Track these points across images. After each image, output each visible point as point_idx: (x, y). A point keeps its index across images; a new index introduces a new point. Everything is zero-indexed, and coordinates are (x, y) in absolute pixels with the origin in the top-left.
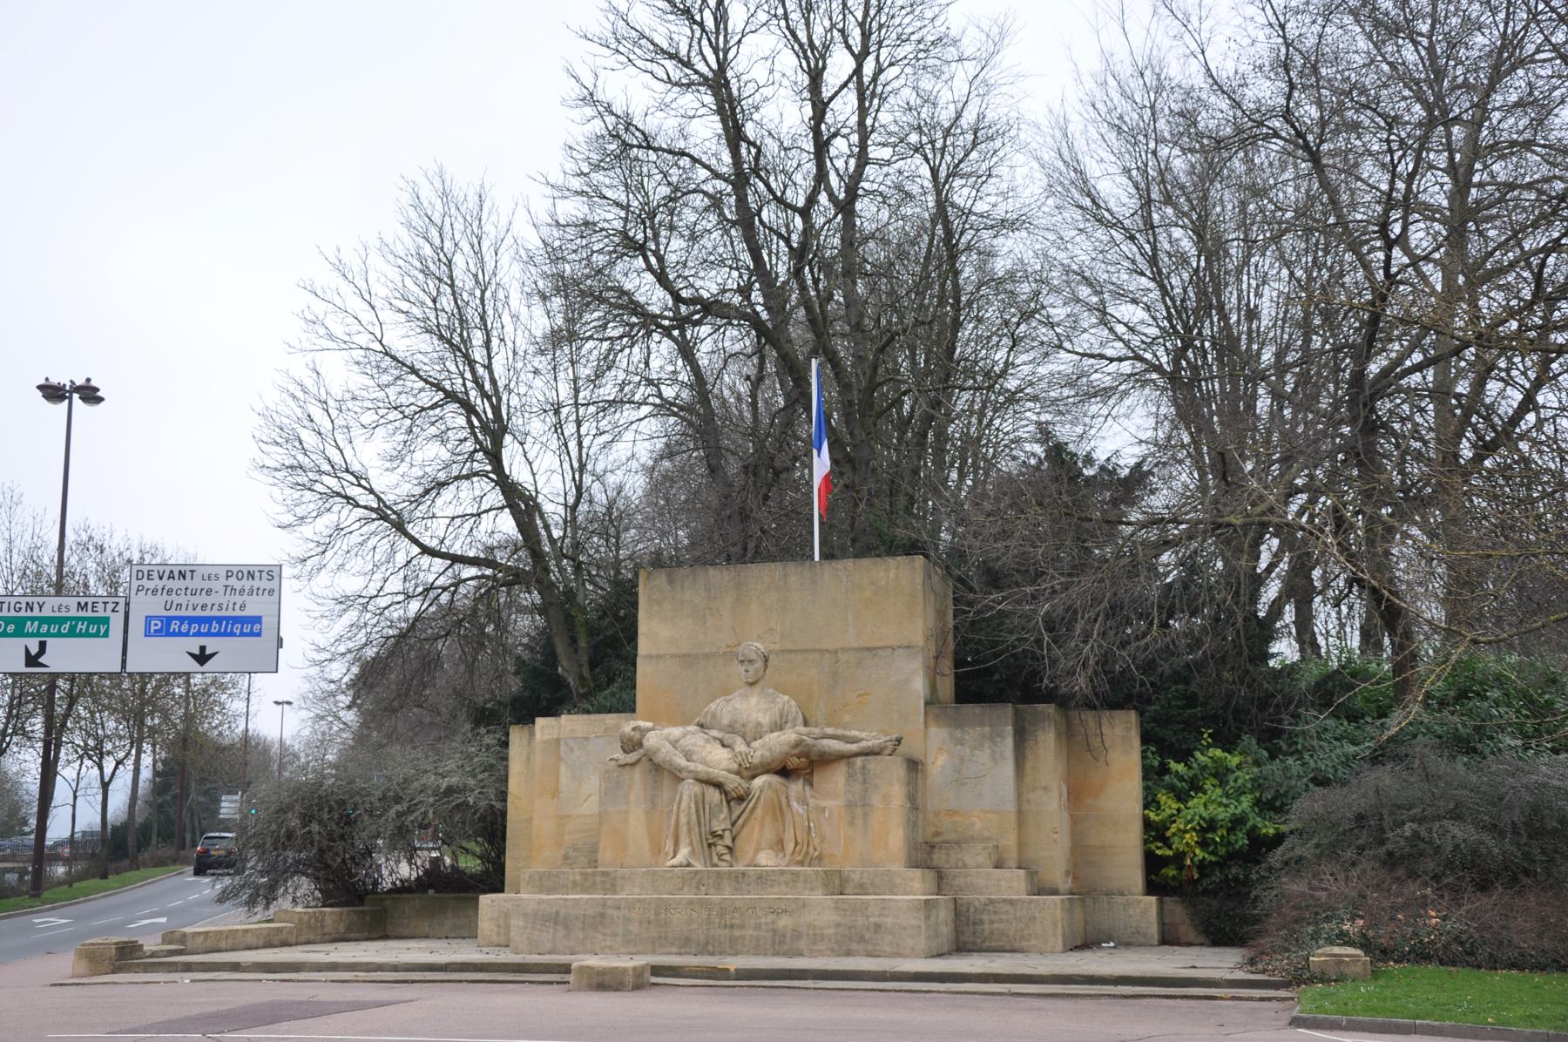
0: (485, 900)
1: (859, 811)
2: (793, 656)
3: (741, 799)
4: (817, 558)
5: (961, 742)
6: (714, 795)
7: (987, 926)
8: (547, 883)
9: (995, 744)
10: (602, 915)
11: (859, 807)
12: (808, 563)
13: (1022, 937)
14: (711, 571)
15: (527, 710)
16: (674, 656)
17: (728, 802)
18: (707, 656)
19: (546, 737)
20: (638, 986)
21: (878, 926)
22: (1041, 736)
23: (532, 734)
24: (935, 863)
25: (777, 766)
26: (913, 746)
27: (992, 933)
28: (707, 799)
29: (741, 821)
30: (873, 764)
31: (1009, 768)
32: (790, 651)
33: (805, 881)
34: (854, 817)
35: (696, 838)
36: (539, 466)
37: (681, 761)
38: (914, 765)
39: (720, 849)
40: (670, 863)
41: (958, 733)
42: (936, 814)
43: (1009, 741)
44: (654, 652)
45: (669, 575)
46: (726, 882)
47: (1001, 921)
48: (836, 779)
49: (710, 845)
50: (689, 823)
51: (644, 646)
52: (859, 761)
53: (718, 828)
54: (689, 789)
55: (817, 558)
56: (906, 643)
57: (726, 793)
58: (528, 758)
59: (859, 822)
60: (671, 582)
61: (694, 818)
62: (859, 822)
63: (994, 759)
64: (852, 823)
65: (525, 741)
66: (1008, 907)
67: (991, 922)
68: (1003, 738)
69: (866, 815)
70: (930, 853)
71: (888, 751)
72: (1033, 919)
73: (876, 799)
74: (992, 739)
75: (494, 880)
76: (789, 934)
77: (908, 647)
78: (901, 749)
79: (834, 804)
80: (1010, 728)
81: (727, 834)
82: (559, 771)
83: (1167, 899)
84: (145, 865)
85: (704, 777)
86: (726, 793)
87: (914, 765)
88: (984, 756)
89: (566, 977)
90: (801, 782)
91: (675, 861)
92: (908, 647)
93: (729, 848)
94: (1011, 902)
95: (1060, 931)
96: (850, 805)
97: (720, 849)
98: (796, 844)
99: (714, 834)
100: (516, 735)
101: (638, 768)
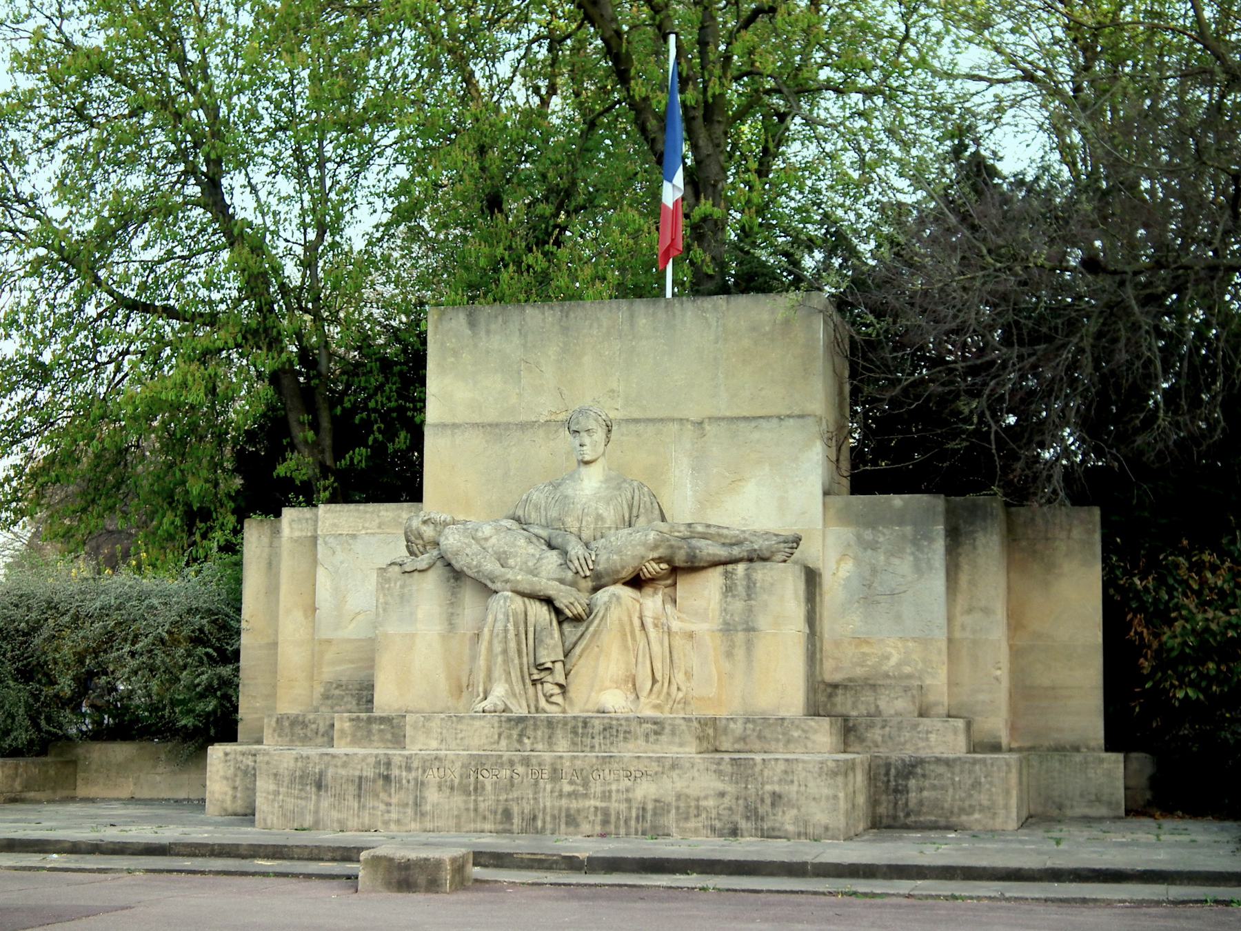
0: (216, 752)
1: (740, 637)
2: (641, 427)
3: (577, 619)
4: (669, 294)
5: (873, 546)
6: (540, 612)
7: (912, 795)
8: (295, 728)
9: (919, 548)
10: (387, 778)
11: (740, 631)
12: (662, 303)
13: (962, 810)
14: (529, 310)
15: (266, 496)
16: (475, 425)
17: (560, 623)
18: (523, 426)
19: (297, 534)
20: (461, 882)
21: (776, 798)
22: (981, 539)
23: (276, 532)
24: (839, 709)
25: (626, 574)
26: (811, 551)
27: (921, 803)
28: (531, 619)
29: (578, 650)
30: (762, 573)
31: (938, 582)
32: (636, 421)
33: (673, 733)
34: (732, 646)
35: (515, 674)
36: (261, 192)
37: (490, 566)
38: (812, 578)
39: (550, 688)
40: (480, 707)
41: (868, 535)
42: (837, 644)
43: (940, 545)
44: (448, 419)
45: (470, 315)
46: (559, 733)
47: (934, 787)
48: (705, 592)
49: (534, 682)
50: (505, 652)
51: (433, 413)
52: (741, 568)
53: (545, 658)
54: (506, 605)
55: (669, 294)
56: (797, 412)
57: (558, 612)
58: (270, 564)
59: (740, 653)
60: (472, 324)
61: (513, 645)
62: (740, 653)
63: (917, 568)
64: (729, 655)
65: (265, 540)
66: (941, 769)
67: (921, 790)
68: (931, 540)
69: (749, 645)
70: (830, 696)
71: (780, 557)
72: (976, 785)
73: (763, 622)
74: (915, 542)
75: (225, 727)
76: (650, 806)
77: (801, 416)
78: (797, 553)
79: (705, 628)
80: (940, 528)
81: (559, 666)
82: (321, 584)
83: (1134, 755)
84: (307, 495)
85: (526, 588)
86: (558, 612)
87: (812, 578)
88: (904, 565)
89: (349, 867)
90: (659, 597)
91: (487, 704)
92: (801, 416)
93: (561, 686)
94: (948, 763)
95: (1014, 801)
96: (728, 629)
97: (550, 688)
98: (654, 681)
99: (541, 668)
100: (254, 535)
101: (430, 573)
